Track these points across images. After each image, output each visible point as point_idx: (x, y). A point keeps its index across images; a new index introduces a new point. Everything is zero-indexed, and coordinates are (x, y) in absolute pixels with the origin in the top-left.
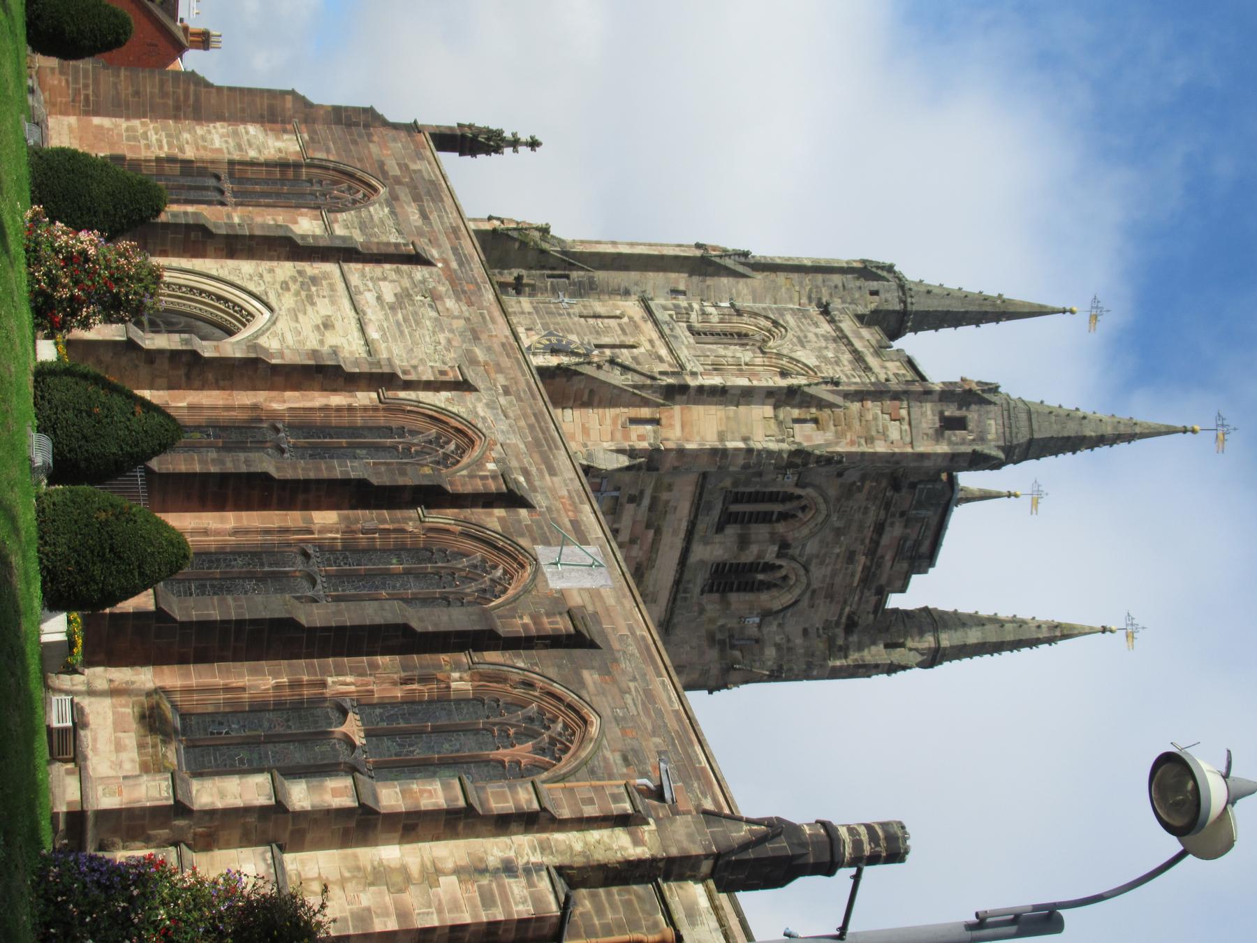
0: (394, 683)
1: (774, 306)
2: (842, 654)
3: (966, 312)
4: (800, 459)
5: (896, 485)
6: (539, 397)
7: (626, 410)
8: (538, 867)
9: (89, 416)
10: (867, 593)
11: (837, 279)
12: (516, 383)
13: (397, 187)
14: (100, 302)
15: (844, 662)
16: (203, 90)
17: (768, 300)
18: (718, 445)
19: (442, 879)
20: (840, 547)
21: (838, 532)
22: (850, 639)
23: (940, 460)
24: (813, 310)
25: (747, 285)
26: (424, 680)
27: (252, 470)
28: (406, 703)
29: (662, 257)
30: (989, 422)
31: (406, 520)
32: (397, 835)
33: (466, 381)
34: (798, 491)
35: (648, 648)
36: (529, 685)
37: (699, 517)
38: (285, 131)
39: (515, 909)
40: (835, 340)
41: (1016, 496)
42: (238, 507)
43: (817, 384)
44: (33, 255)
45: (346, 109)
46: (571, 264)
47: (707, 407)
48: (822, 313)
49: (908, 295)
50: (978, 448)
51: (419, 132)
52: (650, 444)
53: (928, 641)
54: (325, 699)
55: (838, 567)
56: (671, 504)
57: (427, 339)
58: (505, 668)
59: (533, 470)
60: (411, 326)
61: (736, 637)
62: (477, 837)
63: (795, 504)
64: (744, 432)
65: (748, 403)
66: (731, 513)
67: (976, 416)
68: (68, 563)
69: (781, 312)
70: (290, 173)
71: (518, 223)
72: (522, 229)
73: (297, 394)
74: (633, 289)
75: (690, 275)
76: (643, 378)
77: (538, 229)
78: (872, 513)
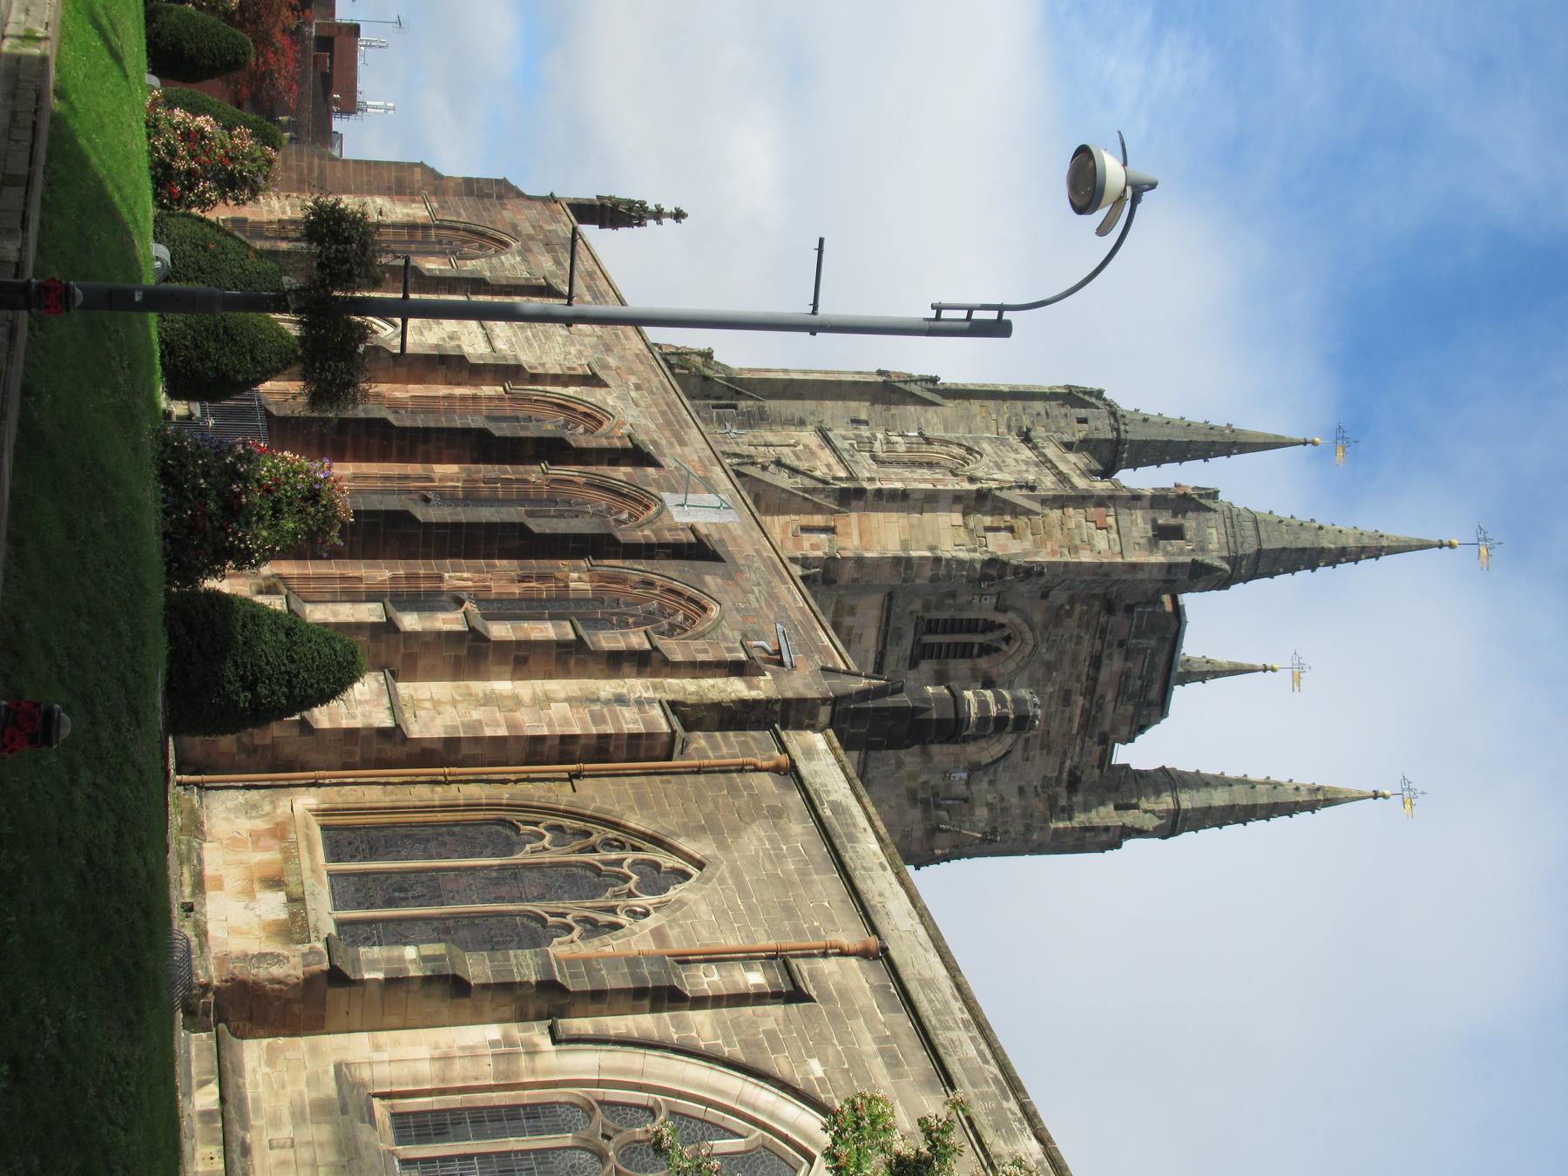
0: (512, 581)
1: (968, 435)
2: (1066, 815)
3: (1191, 442)
4: (995, 565)
5: (1110, 609)
6: (672, 392)
7: (797, 517)
8: (650, 701)
9: (206, 251)
10: (1089, 742)
11: (1039, 406)
12: (649, 382)
13: (530, 242)
14: (215, 178)
15: (1068, 824)
16: (328, 163)
17: (961, 429)
18: (902, 554)
19: (553, 705)
20: (1053, 685)
21: (1050, 667)
22: (1074, 799)
23: (1155, 571)
24: (1013, 439)
25: (936, 413)
26: (541, 578)
27: (370, 416)
28: (525, 600)
29: (839, 383)
30: (1210, 530)
31: (528, 473)
32: (509, 668)
33: (595, 375)
34: (1000, 618)
35: (774, 565)
36: (649, 584)
37: (888, 648)
38: (414, 201)
39: (625, 726)
40: (1036, 465)
41: (1273, 670)
42: (357, 458)
43: (1010, 488)
44: (153, 127)
45: (478, 180)
46: (738, 393)
47: (887, 514)
48: (1022, 441)
49: (1121, 422)
50: (1200, 558)
51: (556, 202)
52: (825, 553)
53: (1166, 802)
54: (442, 593)
55: (1053, 709)
56: (854, 631)
57: (557, 350)
58: (625, 571)
59: (664, 442)
60: (540, 340)
61: (941, 795)
62: (590, 678)
63: (997, 634)
64: (930, 540)
65: (933, 511)
66: (925, 645)
67: (1194, 524)
68: (185, 337)
69: (977, 442)
70: (419, 234)
71: (678, 349)
72: (681, 354)
73: (421, 386)
74: (810, 419)
75: (873, 404)
76: (813, 482)
77: (700, 354)
78: (1086, 643)
